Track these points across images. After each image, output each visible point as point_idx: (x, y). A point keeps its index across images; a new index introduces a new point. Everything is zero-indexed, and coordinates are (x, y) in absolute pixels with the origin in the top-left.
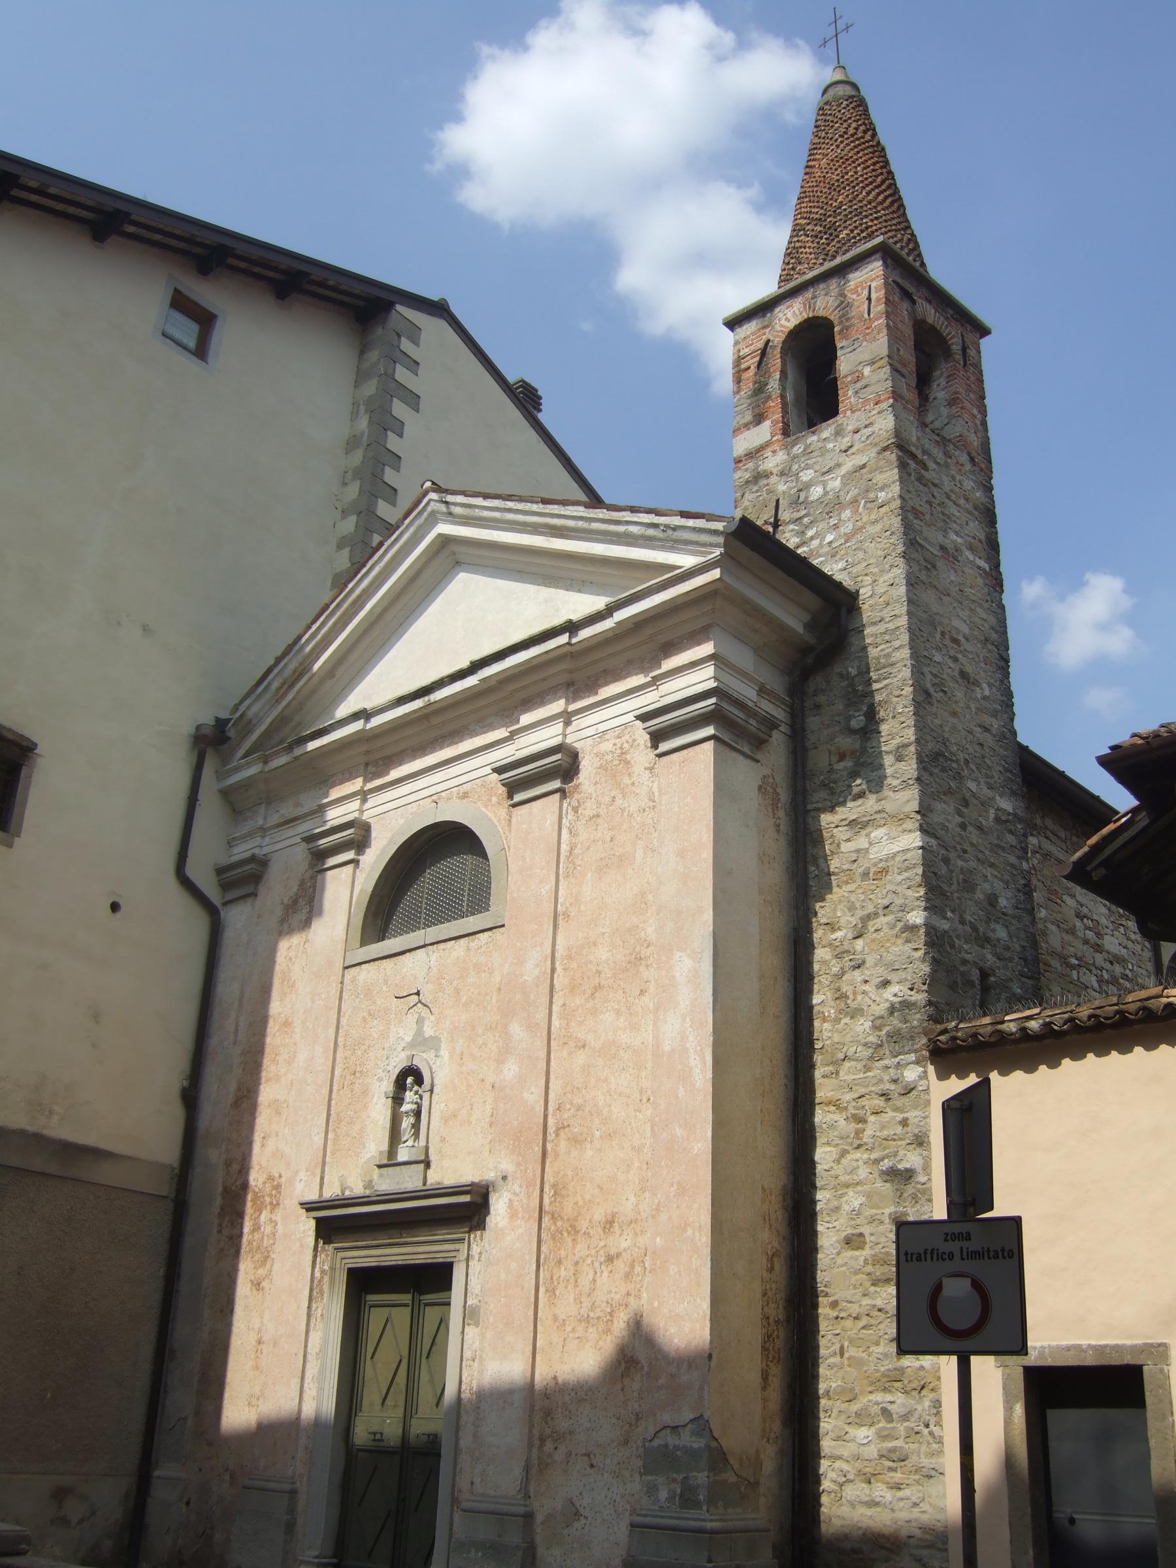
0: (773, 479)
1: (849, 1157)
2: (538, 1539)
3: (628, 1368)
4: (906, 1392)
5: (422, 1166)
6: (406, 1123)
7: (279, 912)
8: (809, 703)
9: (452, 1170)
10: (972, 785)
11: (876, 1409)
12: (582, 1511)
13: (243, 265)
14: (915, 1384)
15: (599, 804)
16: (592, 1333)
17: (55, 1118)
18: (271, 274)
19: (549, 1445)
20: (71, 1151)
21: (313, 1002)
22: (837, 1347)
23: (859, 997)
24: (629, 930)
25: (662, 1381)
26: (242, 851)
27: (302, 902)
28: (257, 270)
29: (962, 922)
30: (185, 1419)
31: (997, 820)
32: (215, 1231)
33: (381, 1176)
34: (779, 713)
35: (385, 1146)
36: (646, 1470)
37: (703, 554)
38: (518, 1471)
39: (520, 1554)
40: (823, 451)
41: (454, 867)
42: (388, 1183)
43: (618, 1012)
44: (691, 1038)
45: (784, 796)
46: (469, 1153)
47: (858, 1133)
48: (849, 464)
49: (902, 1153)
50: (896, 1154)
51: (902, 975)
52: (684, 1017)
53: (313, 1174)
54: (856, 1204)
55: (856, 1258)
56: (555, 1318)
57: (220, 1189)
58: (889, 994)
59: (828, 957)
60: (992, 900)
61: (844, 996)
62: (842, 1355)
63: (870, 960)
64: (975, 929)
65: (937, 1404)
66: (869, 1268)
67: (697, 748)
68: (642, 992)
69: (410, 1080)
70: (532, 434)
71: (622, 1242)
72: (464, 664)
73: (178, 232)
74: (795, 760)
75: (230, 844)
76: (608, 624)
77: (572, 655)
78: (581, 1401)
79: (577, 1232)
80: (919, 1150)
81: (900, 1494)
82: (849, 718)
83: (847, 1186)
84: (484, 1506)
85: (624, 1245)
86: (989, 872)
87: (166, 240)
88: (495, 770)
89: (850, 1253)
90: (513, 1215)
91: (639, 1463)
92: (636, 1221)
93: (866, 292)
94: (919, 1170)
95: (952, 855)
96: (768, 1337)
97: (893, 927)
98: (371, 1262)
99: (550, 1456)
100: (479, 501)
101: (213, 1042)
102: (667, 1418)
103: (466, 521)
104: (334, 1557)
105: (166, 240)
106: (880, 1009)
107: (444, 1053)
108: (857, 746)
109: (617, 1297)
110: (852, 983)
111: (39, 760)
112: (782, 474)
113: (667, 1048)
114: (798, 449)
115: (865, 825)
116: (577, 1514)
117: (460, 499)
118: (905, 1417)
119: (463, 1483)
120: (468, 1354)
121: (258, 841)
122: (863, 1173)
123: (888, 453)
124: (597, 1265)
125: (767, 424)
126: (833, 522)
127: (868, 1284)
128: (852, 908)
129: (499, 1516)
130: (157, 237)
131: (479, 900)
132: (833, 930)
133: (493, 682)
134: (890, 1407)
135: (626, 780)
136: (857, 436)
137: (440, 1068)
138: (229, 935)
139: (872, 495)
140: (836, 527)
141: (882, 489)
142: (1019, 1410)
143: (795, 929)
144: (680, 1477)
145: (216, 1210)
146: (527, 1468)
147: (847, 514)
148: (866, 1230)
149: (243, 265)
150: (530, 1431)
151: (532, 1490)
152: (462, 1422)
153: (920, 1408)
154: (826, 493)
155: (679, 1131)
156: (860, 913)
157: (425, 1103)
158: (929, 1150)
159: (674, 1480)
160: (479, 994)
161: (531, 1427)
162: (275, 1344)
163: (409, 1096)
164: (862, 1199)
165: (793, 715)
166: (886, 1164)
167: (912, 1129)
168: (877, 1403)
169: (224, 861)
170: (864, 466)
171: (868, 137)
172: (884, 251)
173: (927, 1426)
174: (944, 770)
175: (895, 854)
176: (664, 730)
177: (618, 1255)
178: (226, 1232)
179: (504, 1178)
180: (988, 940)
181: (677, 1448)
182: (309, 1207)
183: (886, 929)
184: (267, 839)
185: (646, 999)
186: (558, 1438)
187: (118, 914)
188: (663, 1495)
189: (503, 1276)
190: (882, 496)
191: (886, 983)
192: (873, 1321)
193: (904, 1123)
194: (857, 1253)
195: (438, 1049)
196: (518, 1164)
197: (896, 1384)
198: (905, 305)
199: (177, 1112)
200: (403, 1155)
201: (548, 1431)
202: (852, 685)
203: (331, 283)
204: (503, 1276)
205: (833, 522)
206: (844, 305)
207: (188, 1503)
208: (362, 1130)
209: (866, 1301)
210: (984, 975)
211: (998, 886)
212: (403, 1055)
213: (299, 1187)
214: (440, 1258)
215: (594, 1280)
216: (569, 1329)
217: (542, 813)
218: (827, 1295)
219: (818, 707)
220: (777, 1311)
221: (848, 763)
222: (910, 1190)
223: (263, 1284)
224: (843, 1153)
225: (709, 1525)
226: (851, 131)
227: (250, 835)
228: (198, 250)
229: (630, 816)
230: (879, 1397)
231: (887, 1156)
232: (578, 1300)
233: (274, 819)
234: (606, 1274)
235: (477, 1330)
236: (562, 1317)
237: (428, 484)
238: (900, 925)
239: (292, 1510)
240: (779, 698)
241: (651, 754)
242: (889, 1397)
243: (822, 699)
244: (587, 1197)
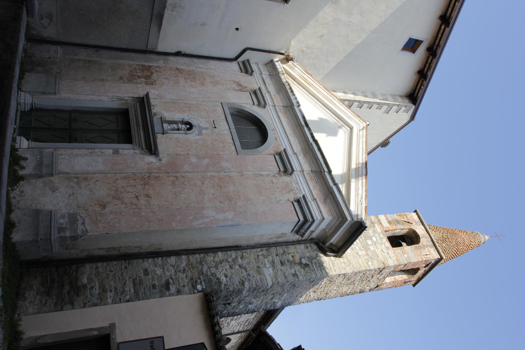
0: (372, 228)
1: (172, 269)
2: (44, 178)
3: (102, 205)
4: (99, 294)
5: (162, 132)
6: (175, 126)
7: (237, 80)
8: (308, 245)
9: (162, 141)
10: (285, 295)
11: (93, 285)
13: (429, 61)
14: (102, 297)
15: (276, 183)
16: (113, 193)
17: (171, 12)
18: (426, 69)
19: (76, 180)
20: (160, 18)
21: (211, 93)
22: (112, 269)
23: (221, 268)
24: (239, 196)
25: (99, 217)
26: (254, 67)
27: (240, 87)
28: (427, 65)
29: (245, 297)
30: (77, 56)
31: (274, 302)
32: (138, 63)
33: (158, 118)
34: (305, 237)
35: (167, 119)
36: (70, 215)
38: (66, 170)
39: (39, 173)
40: (381, 244)
41: (254, 134)
42: (156, 120)
43: (214, 194)
44: (208, 220)
45: (280, 240)
47: (180, 271)
48: (378, 252)
49: (175, 286)
50: (174, 284)
51: (229, 282)
52: (214, 217)
53: (157, 96)
54: (158, 272)
55: (141, 273)
56: (117, 180)
57: (151, 65)
58: (223, 279)
59: (233, 257)
60: (251, 303)
61: (221, 263)
62: (110, 271)
63: (233, 271)
64: (242, 300)
66: (138, 278)
68: (220, 202)
69: (188, 126)
70: (374, 146)
71: (143, 201)
73: (441, 42)
74: (292, 242)
75: (257, 64)
76: (331, 184)
77: (321, 172)
78: (91, 190)
79: (145, 185)
80: (176, 292)
81: (66, 295)
82: (304, 258)
83: (163, 269)
84: (54, 160)
85: (142, 202)
86: (259, 302)
87: (438, 38)
88: (285, 150)
89: (142, 271)
90: (149, 163)
91: (72, 212)
92: (149, 205)
93: (428, 254)
94: (170, 292)
95: (265, 292)
96: (114, 248)
97: (243, 277)
98: (131, 117)
99: (72, 181)
100: (364, 140)
101: (196, 60)
102: (87, 220)
103: (358, 136)
104: (35, 108)
105: (438, 38)
106: (218, 275)
107: (198, 137)
108: (297, 261)
109: (125, 201)
110: (226, 265)
111: (283, 4)
112: (374, 231)
113: (204, 212)
114: (382, 236)
115: (273, 266)
116: (53, 191)
117: (365, 133)
118: (91, 294)
119: (62, 151)
120: (104, 151)
121: (258, 72)
122: (168, 274)
123: (382, 264)
124: (135, 193)
125: (388, 225)
126: (362, 248)
127: (133, 278)
128: (248, 263)
129: (51, 165)
130: (440, 35)
131: (245, 146)
132: (241, 258)
133: (311, 147)
134: (94, 289)
135: (284, 192)
136: (387, 254)
137: (192, 136)
138: (228, 64)
139: (370, 260)
140: (360, 249)
141: (372, 263)
142: (96, 333)
143: (240, 246)
144: (68, 226)
145: (144, 63)
146: (68, 173)
147: (364, 253)
148: (150, 276)
149: (429, 61)
150: (79, 174)
151: (61, 175)
152: (81, 150)
153: (94, 299)
154: (369, 245)
155: (178, 218)
156: (247, 266)
157: (182, 132)
158: (176, 295)
159: (66, 225)
161: (82, 174)
162: (102, 85)
163: (184, 126)
164: (159, 274)
165: (304, 240)
166: (171, 281)
167: (182, 289)
168: (95, 284)
169: (251, 62)
170: (378, 257)
171: (470, 248)
172: (441, 258)
173: (89, 302)
174: (290, 288)
175: (265, 276)
176: (300, 203)
177: (138, 200)
178: (137, 67)
179: (160, 160)
180: (239, 303)
181: (77, 224)
182: (147, 95)
183: (242, 275)
184: (258, 75)
185: (219, 203)
186: (78, 183)
187: (235, 30)
188: (62, 221)
189: (129, 161)
190: (370, 263)
191: (226, 276)
192: (121, 280)
193: (184, 286)
194: (142, 274)
195: (199, 135)
196: (165, 164)
197: (101, 290)
198: (424, 265)
199: (174, 51)
200: (165, 125)
201: (80, 180)
202: (315, 258)
203: (422, 87)
204: (129, 161)
205: (362, 248)
206: (424, 247)
207: (50, 58)
208: (172, 111)
209: (127, 278)
210: (229, 304)
211: (255, 305)
212: (196, 124)
213: (153, 91)
214: (133, 139)
215: (130, 192)
216: (114, 184)
217: (272, 166)
218: (129, 264)
219: (307, 248)
220: (122, 251)
221: (291, 259)
222: (163, 290)
223: (122, 80)
224: (173, 266)
225: (52, 238)
226: (472, 243)
227: (259, 70)
228: (435, 47)
229: (274, 194)
230: (97, 285)
231: (173, 281)
232: (123, 187)
233: (265, 78)
234: (132, 196)
235: (111, 153)
237: (368, 123)
238: (244, 279)
239: (49, 93)
240: (309, 236)
241: (292, 200)
242: (97, 288)
243: (309, 249)
244: (156, 188)
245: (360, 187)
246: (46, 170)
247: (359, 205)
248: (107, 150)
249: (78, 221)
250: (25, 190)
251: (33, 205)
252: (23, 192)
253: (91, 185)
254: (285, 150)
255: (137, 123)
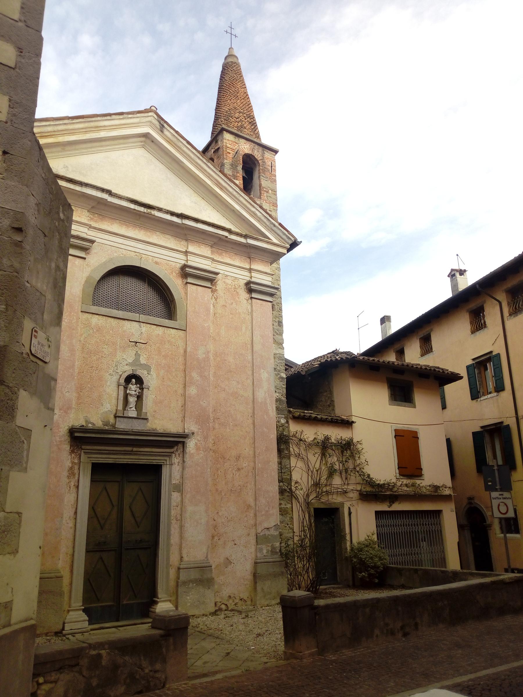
3: (248, 508)
12: (232, 561)
19: (216, 538)
25: (263, 513)
37: (279, 240)
44: (268, 400)
46: (171, 420)
56: (217, 490)
65: (292, 518)
67: (266, 303)
72: (179, 211)
76: (242, 240)
79: (224, 458)
84: (192, 566)
85: (244, 465)
90: (198, 448)
98: (110, 461)
102: (266, 525)
124: (234, 471)
137: (151, 380)
144: (270, 545)
155: (265, 430)
159: (268, 546)
160: (172, 354)
179: (193, 433)
188: (265, 551)
201: (216, 533)
214: (155, 462)
215: (233, 477)
232: (226, 484)
236: (220, 490)
238: (279, 376)
245: (253, 209)
246: (203, 576)
247: (274, 228)
248: (170, 500)
249: (265, 535)
250: (228, 595)
251: (246, 583)
252: (230, 597)
253: (223, 520)
254: (473, 359)
255: (126, 453)
